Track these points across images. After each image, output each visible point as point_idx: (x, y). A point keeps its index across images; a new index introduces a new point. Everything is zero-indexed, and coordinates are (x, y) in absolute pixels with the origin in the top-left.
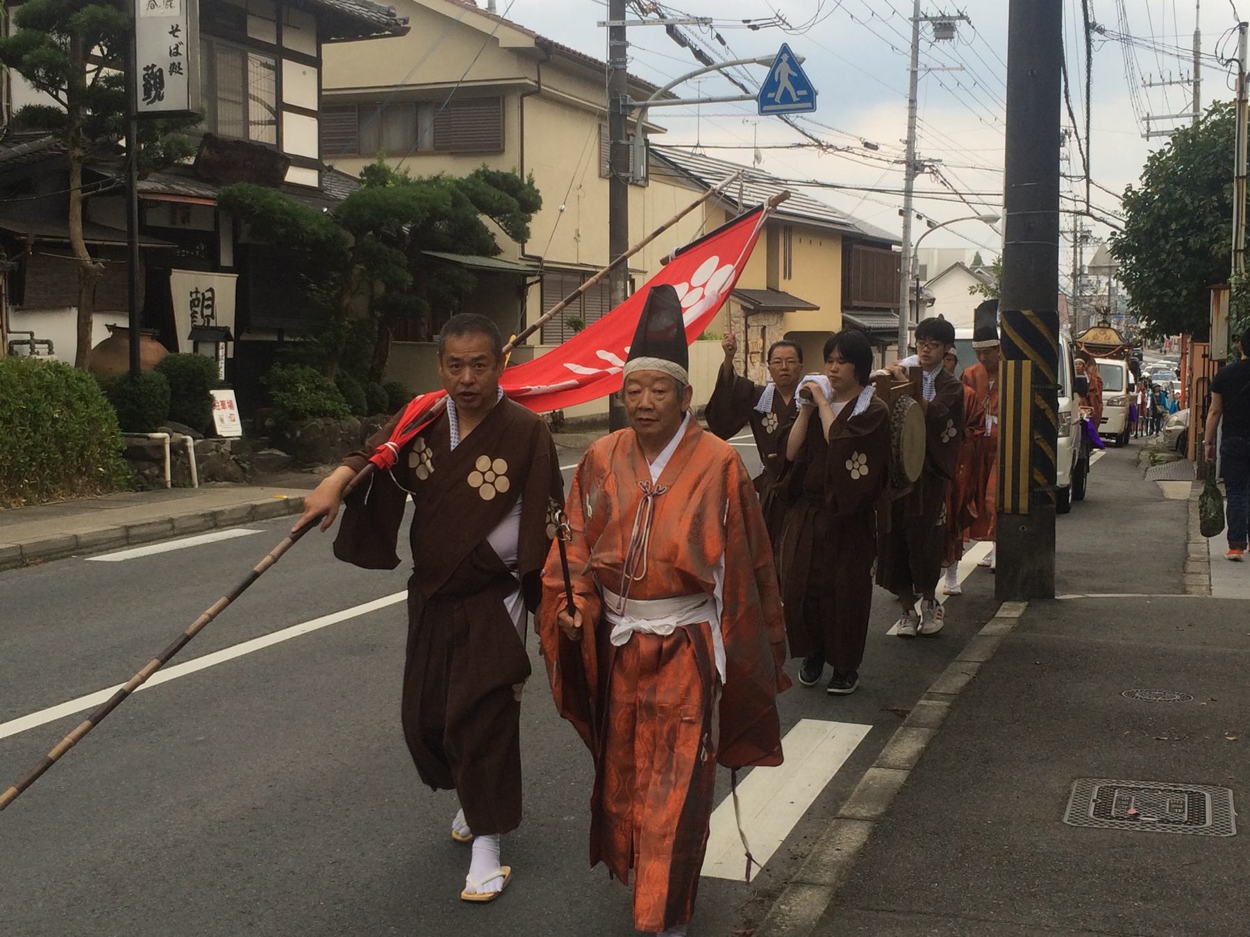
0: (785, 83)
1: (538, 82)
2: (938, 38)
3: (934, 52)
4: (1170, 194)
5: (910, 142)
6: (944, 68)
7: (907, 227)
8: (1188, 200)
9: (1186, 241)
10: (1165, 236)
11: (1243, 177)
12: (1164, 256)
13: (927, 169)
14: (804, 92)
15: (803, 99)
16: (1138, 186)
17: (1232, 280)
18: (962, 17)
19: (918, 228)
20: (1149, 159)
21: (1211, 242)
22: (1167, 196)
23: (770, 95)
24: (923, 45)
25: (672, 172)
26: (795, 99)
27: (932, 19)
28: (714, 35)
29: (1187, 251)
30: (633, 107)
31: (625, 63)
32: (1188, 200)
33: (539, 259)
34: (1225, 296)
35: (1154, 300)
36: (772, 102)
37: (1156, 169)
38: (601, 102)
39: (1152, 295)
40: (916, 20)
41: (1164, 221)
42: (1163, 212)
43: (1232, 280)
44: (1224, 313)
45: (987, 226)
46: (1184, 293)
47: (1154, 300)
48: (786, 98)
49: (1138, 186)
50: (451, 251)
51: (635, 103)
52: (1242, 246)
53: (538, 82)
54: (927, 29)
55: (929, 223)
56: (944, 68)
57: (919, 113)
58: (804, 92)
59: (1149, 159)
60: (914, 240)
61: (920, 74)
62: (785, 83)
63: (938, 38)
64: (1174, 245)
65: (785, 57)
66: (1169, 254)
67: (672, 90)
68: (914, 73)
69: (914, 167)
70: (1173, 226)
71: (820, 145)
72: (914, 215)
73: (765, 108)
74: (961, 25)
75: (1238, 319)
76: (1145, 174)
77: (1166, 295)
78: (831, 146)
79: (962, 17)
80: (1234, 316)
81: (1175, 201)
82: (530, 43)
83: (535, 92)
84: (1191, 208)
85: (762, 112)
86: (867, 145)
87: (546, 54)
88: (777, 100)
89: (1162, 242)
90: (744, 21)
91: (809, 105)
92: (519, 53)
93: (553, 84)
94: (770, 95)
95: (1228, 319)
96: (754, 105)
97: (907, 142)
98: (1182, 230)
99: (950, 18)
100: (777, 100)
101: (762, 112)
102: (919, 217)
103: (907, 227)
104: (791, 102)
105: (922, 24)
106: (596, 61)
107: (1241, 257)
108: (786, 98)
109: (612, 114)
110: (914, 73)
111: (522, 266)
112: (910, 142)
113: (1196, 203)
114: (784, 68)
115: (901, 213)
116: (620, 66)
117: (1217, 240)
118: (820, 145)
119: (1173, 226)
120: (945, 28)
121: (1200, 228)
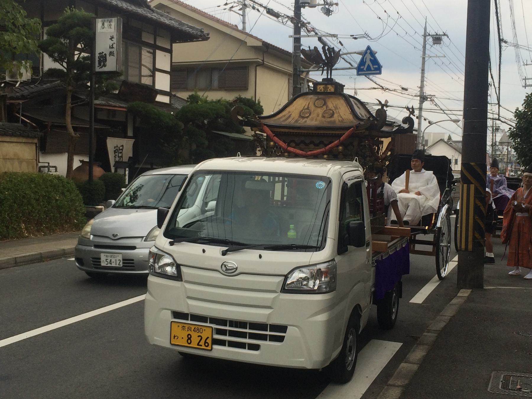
0: (368, 62)
1: (263, 60)
3: (433, 49)
5: (422, 87)
6: (437, 56)
13: (429, 99)
14: (377, 66)
15: (376, 69)
16: (521, 108)
18: (445, 35)
19: (424, 124)
23: (362, 67)
24: (428, 46)
26: (372, 69)
27: (432, 36)
30: (303, 72)
36: (362, 70)
38: (289, 69)
40: (425, 36)
45: (454, 124)
47: (528, 158)
50: (223, 131)
51: (304, 70)
53: (263, 60)
54: (430, 40)
55: (429, 122)
56: (437, 56)
57: (426, 75)
58: (377, 66)
61: (426, 59)
62: (368, 62)
63: (434, 44)
65: (369, 51)
72: (423, 119)
73: (360, 73)
74: (444, 38)
76: (524, 103)
79: (445, 35)
82: (260, 44)
83: (262, 65)
85: (358, 74)
86: (403, 88)
88: (365, 69)
91: (378, 72)
92: (255, 49)
93: (269, 62)
94: (362, 67)
96: (355, 71)
97: (420, 88)
100: (365, 69)
101: (358, 74)
102: (425, 120)
104: (371, 70)
105: (428, 37)
108: (369, 68)
110: (424, 58)
114: (368, 56)
120: (437, 39)
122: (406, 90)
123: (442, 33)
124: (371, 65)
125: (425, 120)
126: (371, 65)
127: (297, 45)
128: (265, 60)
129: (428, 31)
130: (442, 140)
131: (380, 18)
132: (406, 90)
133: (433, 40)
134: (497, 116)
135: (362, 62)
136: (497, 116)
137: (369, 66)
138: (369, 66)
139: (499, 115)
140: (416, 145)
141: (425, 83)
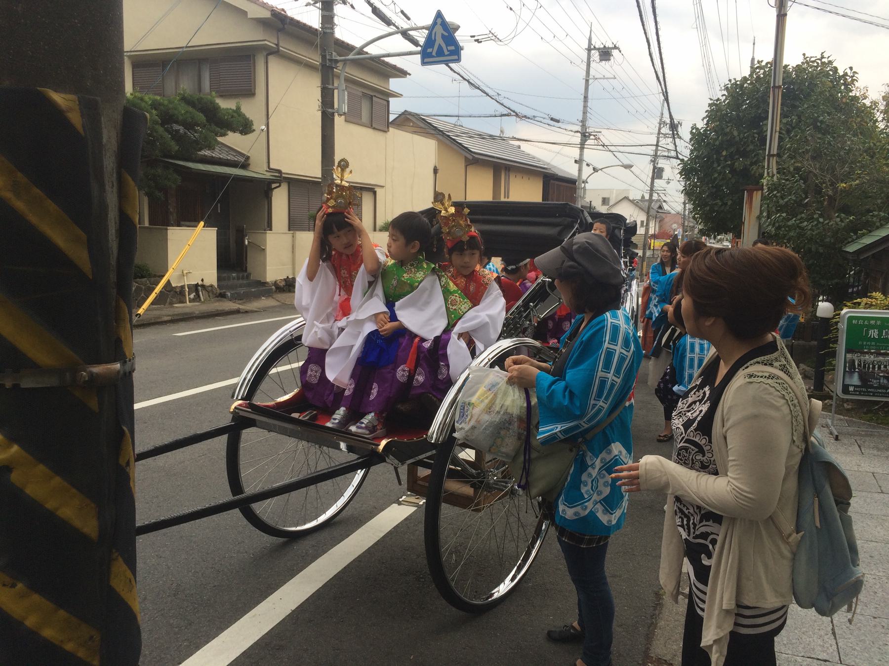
0: (439, 41)
1: (277, 45)
2: (601, 60)
3: (599, 68)
4: (723, 129)
5: (583, 122)
6: (604, 78)
7: (580, 170)
8: (735, 133)
9: (733, 164)
10: (718, 160)
11: (773, 155)
12: (716, 175)
13: (592, 137)
14: (453, 48)
15: (452, 53)
16: (701, 125)
17: (764, 182)
18: (615, 47)
19: (587, 171)
20: (710, 105)
21: (752, 164)
22: (718, 130)
23: (429, 50)
24: (593, 65)
25: (433, 132)
26: (446, 53)
27: (599, 49)
28: (398, 10)
29: (733, 171)
30: (337, 61)
31: (332, 29)
32: (735, 133)
33: (279, 171)
34: (757, 197)
35: (708, 208)
36: (430, 55)
37: (716, 112)
38: (316, 59)
39: (706, 205)
40: (589, 50)
41: (718, 151)
42: (717, 143)
43: (764, 182)
44: (756, 211)
45: (627, 171)
46: (730, 203)
47: (708, 208)
48: (440, 53)
49: (701, 125)
50: (180, 159)
51: (339, 58)
52: (775, 151)
53: (277, 45)
54: (595, 55)
55: (594, 169)
56: (604, 78)
57: (589, 104)
58: (453, 48)
59: (710, 105)
60: (584, 177)
61: (590, 81)
62: (439, 41)
63: (601, 60)
64: (724, 167)
65: (439, 21)
66: (720, 174)
67: (365, 50)
68: (587, 81)
69: (585, 136)
70: (724, 153)
71: (517, 115)
72: (584, 164)
73: (426, 60)
74: (615, 53)
75: (768, 217)
76: (707, 116)
77: (716, 204)
78: (525, 116)
79: (615, 47)
80: (765, 214)
81: (726, 134)
82: (267, 14)
83: (274, 52)
84: (737, 139)
85: (424, 63)
86: (552, 119)
87: (280, 23)
88: (434, 54)
89: (715, 165)
90: (472, 37)
91: (456, 57)
92: (262, 23)
93: (288, 46)
94: (429, 50)
95: (759, 218)
96: (418, 58)
97: (582, 121)
98: (731, 156)
99: (609, 48)
100: (434, 54)
101: (424, 63)
102: (588, 165)
103: (580, 170)
104: (444, 55)
105: (593, 52)
106: (310, 27)
107: (774, 161)
108: (440, 53)
109: (323, 65)
110: (587, 81)
111: (268, 175)
112: (583, 122)
113: (742, 136)
114: (439, 30)
115: (576, 162)
116: (328, 31)
117: (755, 163)
118: (517, 115)
119: (724, 153)
120: (606, 54)
121: (744, 154)
122: (558, 121)
123: (611, 46)
124: (444, 46)
125: (588, 165)
126: (444, 46)
127: (326, 13)
128: (281, 44)
129: (593, 42)
130: (626, 198)
131: (511, 9)
132: (558, 121)
133: (600, 55)
134: (673, 154)
135: (430, 41)
136: (673, 154)
137: (440, 47)
138: (440, 47)
139: (676, 150)
140: (574, 199)
141: (588, 115)
